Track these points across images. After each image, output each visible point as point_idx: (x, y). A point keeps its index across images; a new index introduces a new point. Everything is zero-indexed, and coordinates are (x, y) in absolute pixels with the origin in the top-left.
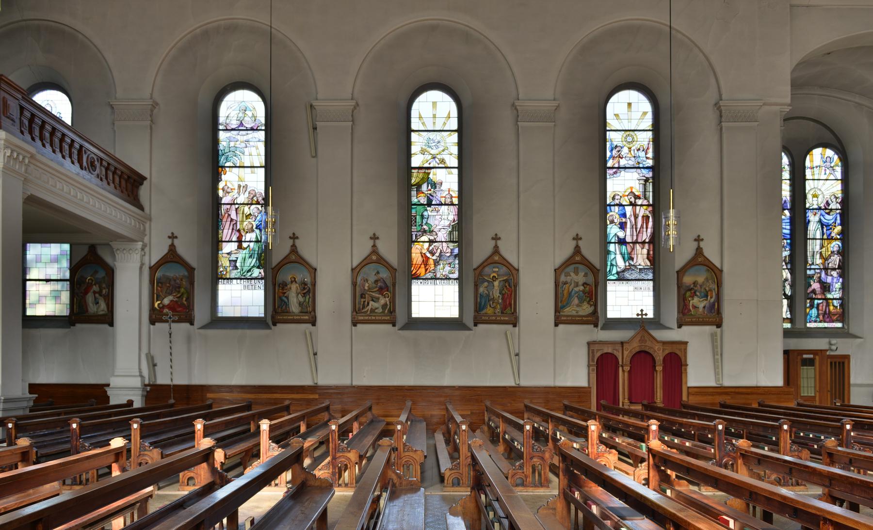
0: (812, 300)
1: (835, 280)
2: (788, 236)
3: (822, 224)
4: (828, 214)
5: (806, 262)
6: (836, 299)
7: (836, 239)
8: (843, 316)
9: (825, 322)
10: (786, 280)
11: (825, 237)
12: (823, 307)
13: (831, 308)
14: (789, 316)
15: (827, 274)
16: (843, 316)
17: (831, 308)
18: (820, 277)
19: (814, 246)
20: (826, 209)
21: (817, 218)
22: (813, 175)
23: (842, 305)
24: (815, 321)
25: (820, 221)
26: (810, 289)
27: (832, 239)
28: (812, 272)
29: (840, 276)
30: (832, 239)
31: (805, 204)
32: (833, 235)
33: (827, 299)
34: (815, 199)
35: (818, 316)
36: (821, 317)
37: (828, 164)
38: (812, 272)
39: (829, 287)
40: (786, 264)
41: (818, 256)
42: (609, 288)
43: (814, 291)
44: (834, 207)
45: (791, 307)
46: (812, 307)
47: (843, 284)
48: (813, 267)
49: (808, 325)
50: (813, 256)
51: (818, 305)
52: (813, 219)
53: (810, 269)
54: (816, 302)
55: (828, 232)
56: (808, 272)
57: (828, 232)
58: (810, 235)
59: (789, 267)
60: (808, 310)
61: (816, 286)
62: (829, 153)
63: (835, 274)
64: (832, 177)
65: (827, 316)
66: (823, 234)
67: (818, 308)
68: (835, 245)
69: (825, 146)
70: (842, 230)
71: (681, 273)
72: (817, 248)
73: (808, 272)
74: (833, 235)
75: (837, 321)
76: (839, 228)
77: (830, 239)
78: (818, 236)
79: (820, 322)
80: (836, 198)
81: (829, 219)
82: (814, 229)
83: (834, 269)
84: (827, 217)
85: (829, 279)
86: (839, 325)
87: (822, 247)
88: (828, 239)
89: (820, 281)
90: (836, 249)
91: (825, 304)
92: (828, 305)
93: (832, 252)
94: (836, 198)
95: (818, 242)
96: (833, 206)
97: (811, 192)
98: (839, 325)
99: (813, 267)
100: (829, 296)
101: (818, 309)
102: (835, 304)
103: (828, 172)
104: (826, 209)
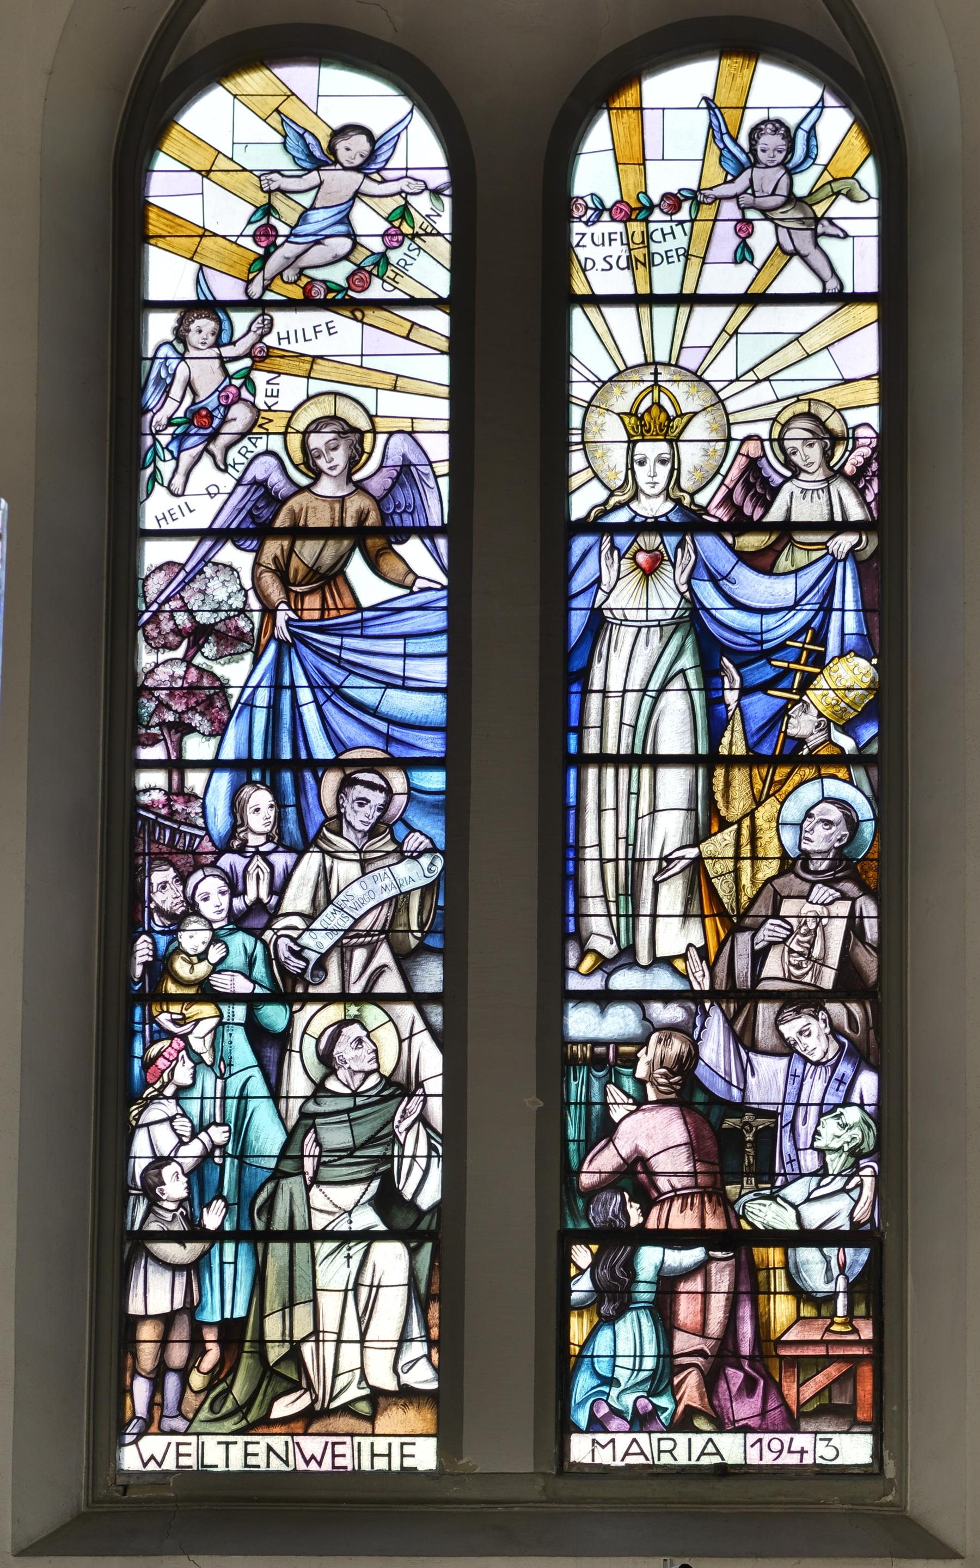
0: (619, 1241)
1: (814, 1089)
2: (433, 744)
3: (708, 644)
4: (762, 563)
5: (559, 924)
6: (819, 1238)
7: (825, 762)
8: (875, 1386)
9: (721, 1424)
10: (401, 1086)
11: (734, 742)
12: (704, 1308)
13: (782, 1309)
14: (422, 1377)
15: (743, 1039)
16: (875, 1386)
17: (782, 1309)
18: (686, 1066)
19: (638, 819)
20: (740, 524)
21: (665, 597)
22: (641, 260)
23: (870, 1289)
24: (641, 1421)
25: (692, 618)
26: (606, 1160)
27: (794, 756)
28: (620, 1022)
29: (859, 1051)
30: (794, 756)
31: (558, 486)
32: (801, 724)
33: (738, 1242)
34: (650, 450)
35: (664, 1376)
36: (691, 1388)
37: (767, 178)
38: (620, 1022)
39: (768, 1138)
40: (405, 960)
41: (672, 896)
42: (445, 678)
43: (635, 1176)
44: (809, 510)
45: (440, 1297)
46: (614, 1298)
47: (887, 1118)
48: (624, 980)
49: (580, 1449)
50: (632, 891)
51: (668, 1284)
52: (634, 601)
53: (604, 999)
54: (649, 1259)
55: (761, 707)
56: (582, 1023)
57: (761, 707)
58: (608, 723)
59: (431, 976)
60: (578, 1329)
61: (655, 1135)
62: (781, 90)
63: (812, 1035)
64: (797, 278)
65: (746, 1367)
66: (717, 726)
67: (663, 1313)
68: (817, 810)
69: (743, 41)
70: (877, 689)
71: (305, 433)
72: (670, 831)
73: (582, 1023)
74: (801, 724)
75: (835, 1411)
76: (852, 674)
77: (780, 757)
78: (674, 735)
79: (684, 1422)
80: (830, 440)
81: (767, 598)
82: (636, 678)
83: (806, 1000)
84: (753, 586)
85: (767, 1080)
86: (855, 1449)
87: (706, 818)
88: (751, 760)
89: (684, 1088)
90: (820, 840)
91: (722, 1279)
92: (750, 1287)
93: (789, 864)
94: (830, 440)
95: (674, 785)
96: (799, 502)
97: (623, 398)
98: (855, 1449)
99: (624, 980)
100: (768, 1215)
101: (666, 1322)
102: (815, 1280)
103: (763, 238)
104: (747, 518)
